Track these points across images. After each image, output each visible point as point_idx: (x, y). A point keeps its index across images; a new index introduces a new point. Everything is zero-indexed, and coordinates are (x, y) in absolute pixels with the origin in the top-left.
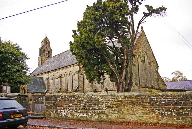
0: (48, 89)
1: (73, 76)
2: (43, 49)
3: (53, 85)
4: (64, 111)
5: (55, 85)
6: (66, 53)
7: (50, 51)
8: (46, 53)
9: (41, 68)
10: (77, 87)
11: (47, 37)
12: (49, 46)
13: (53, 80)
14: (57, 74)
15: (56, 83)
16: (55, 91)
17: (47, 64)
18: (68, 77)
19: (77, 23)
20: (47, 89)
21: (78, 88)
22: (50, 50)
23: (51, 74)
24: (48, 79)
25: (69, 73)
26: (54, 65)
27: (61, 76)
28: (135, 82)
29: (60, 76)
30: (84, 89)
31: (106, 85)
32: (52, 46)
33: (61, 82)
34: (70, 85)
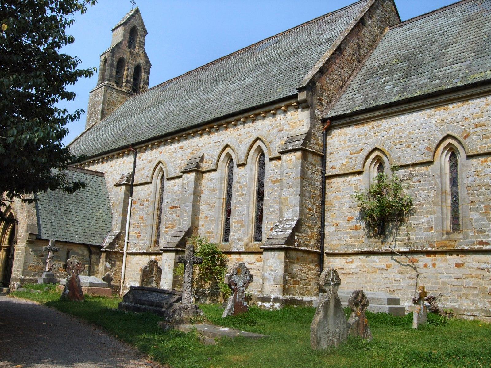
0: (123, 227)
1: (270, 166)
2: (118, 55)
3: (149, 211)
4: (194, 354)
5: (160, 209)
6: (216, 67)
7: (140, 72)
8: (128, 73)
9: (101, 133)
10: (293, 224)
11: (137, 11)
12: (142, 45)
13: (151, 187)
14: (175, 155)
15: (165, 201)
16: (157, 242)
17: (125, 115)
18: (235, 169)
19: (73, 43)
20: (117, 231)
21: (297, 229)
22: (142, 62)
23: (147, 159)
24: (130, 184)
25: (243, 149)
26: (161, 115)
27: (198, 166)
28: (362, 184)
29: (197, 169)
30: (322, 234)
31: (475, 215)
32: (153, 46)
33: (197, 194)
34: (244, 209)
